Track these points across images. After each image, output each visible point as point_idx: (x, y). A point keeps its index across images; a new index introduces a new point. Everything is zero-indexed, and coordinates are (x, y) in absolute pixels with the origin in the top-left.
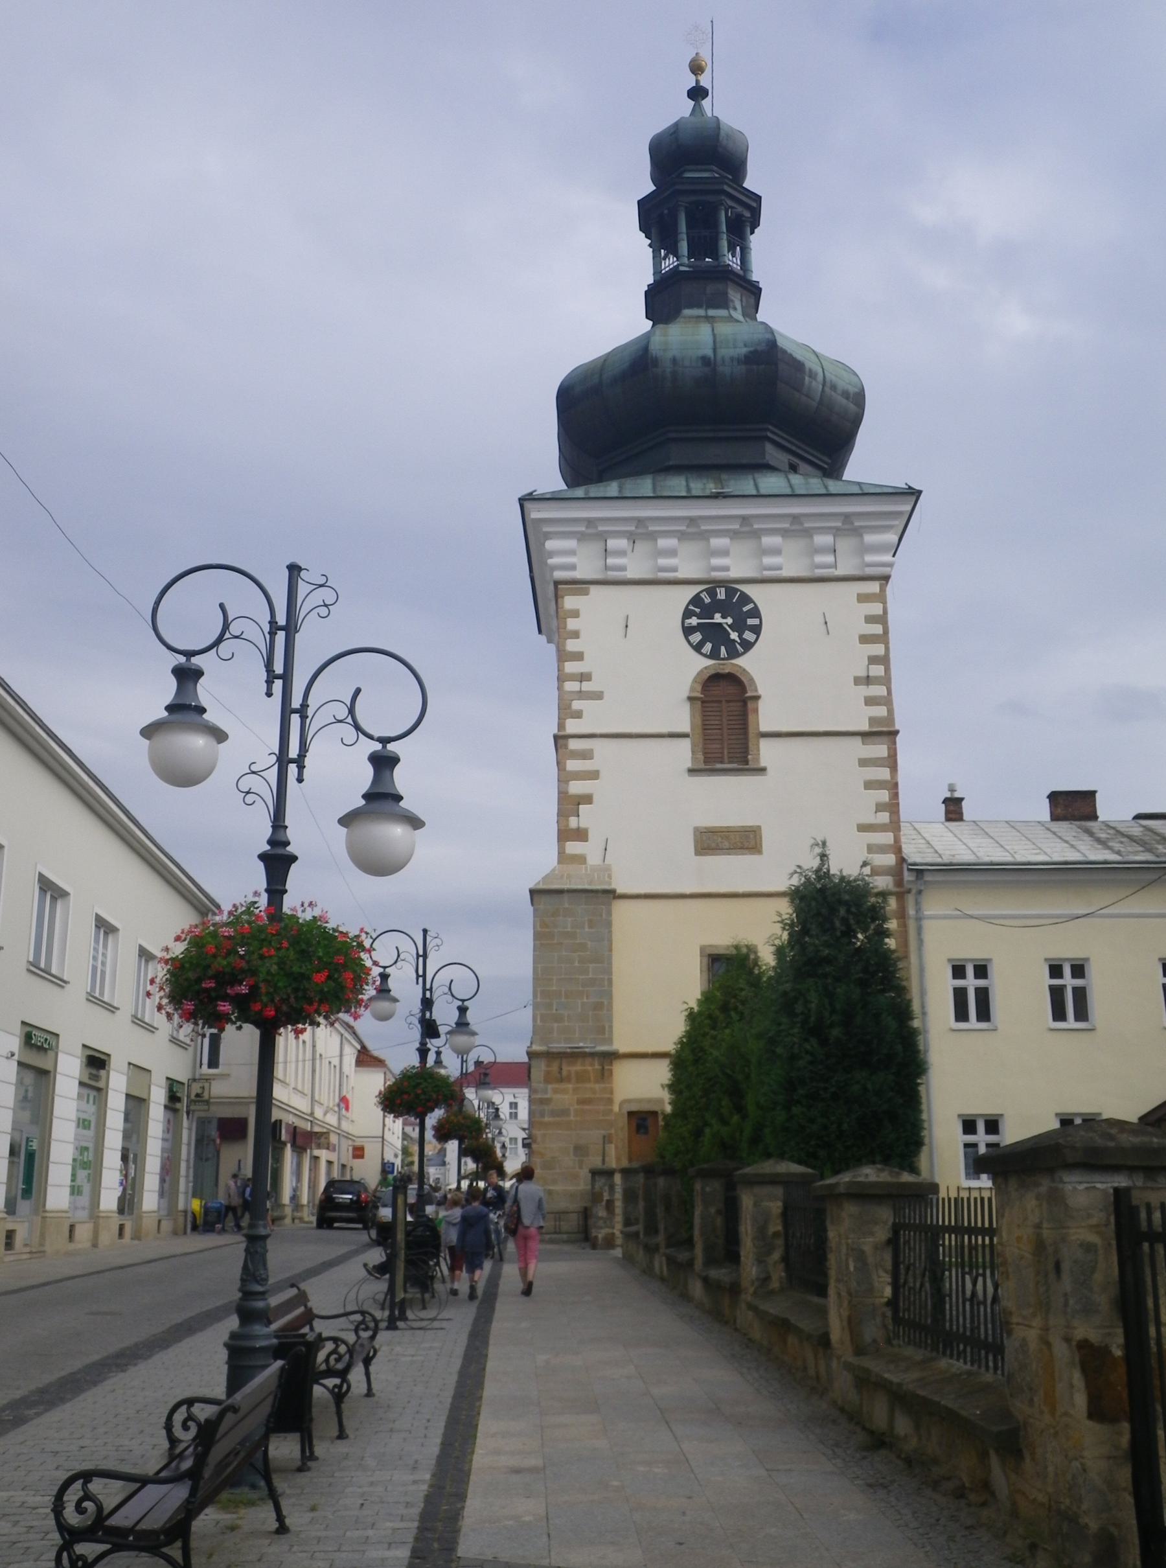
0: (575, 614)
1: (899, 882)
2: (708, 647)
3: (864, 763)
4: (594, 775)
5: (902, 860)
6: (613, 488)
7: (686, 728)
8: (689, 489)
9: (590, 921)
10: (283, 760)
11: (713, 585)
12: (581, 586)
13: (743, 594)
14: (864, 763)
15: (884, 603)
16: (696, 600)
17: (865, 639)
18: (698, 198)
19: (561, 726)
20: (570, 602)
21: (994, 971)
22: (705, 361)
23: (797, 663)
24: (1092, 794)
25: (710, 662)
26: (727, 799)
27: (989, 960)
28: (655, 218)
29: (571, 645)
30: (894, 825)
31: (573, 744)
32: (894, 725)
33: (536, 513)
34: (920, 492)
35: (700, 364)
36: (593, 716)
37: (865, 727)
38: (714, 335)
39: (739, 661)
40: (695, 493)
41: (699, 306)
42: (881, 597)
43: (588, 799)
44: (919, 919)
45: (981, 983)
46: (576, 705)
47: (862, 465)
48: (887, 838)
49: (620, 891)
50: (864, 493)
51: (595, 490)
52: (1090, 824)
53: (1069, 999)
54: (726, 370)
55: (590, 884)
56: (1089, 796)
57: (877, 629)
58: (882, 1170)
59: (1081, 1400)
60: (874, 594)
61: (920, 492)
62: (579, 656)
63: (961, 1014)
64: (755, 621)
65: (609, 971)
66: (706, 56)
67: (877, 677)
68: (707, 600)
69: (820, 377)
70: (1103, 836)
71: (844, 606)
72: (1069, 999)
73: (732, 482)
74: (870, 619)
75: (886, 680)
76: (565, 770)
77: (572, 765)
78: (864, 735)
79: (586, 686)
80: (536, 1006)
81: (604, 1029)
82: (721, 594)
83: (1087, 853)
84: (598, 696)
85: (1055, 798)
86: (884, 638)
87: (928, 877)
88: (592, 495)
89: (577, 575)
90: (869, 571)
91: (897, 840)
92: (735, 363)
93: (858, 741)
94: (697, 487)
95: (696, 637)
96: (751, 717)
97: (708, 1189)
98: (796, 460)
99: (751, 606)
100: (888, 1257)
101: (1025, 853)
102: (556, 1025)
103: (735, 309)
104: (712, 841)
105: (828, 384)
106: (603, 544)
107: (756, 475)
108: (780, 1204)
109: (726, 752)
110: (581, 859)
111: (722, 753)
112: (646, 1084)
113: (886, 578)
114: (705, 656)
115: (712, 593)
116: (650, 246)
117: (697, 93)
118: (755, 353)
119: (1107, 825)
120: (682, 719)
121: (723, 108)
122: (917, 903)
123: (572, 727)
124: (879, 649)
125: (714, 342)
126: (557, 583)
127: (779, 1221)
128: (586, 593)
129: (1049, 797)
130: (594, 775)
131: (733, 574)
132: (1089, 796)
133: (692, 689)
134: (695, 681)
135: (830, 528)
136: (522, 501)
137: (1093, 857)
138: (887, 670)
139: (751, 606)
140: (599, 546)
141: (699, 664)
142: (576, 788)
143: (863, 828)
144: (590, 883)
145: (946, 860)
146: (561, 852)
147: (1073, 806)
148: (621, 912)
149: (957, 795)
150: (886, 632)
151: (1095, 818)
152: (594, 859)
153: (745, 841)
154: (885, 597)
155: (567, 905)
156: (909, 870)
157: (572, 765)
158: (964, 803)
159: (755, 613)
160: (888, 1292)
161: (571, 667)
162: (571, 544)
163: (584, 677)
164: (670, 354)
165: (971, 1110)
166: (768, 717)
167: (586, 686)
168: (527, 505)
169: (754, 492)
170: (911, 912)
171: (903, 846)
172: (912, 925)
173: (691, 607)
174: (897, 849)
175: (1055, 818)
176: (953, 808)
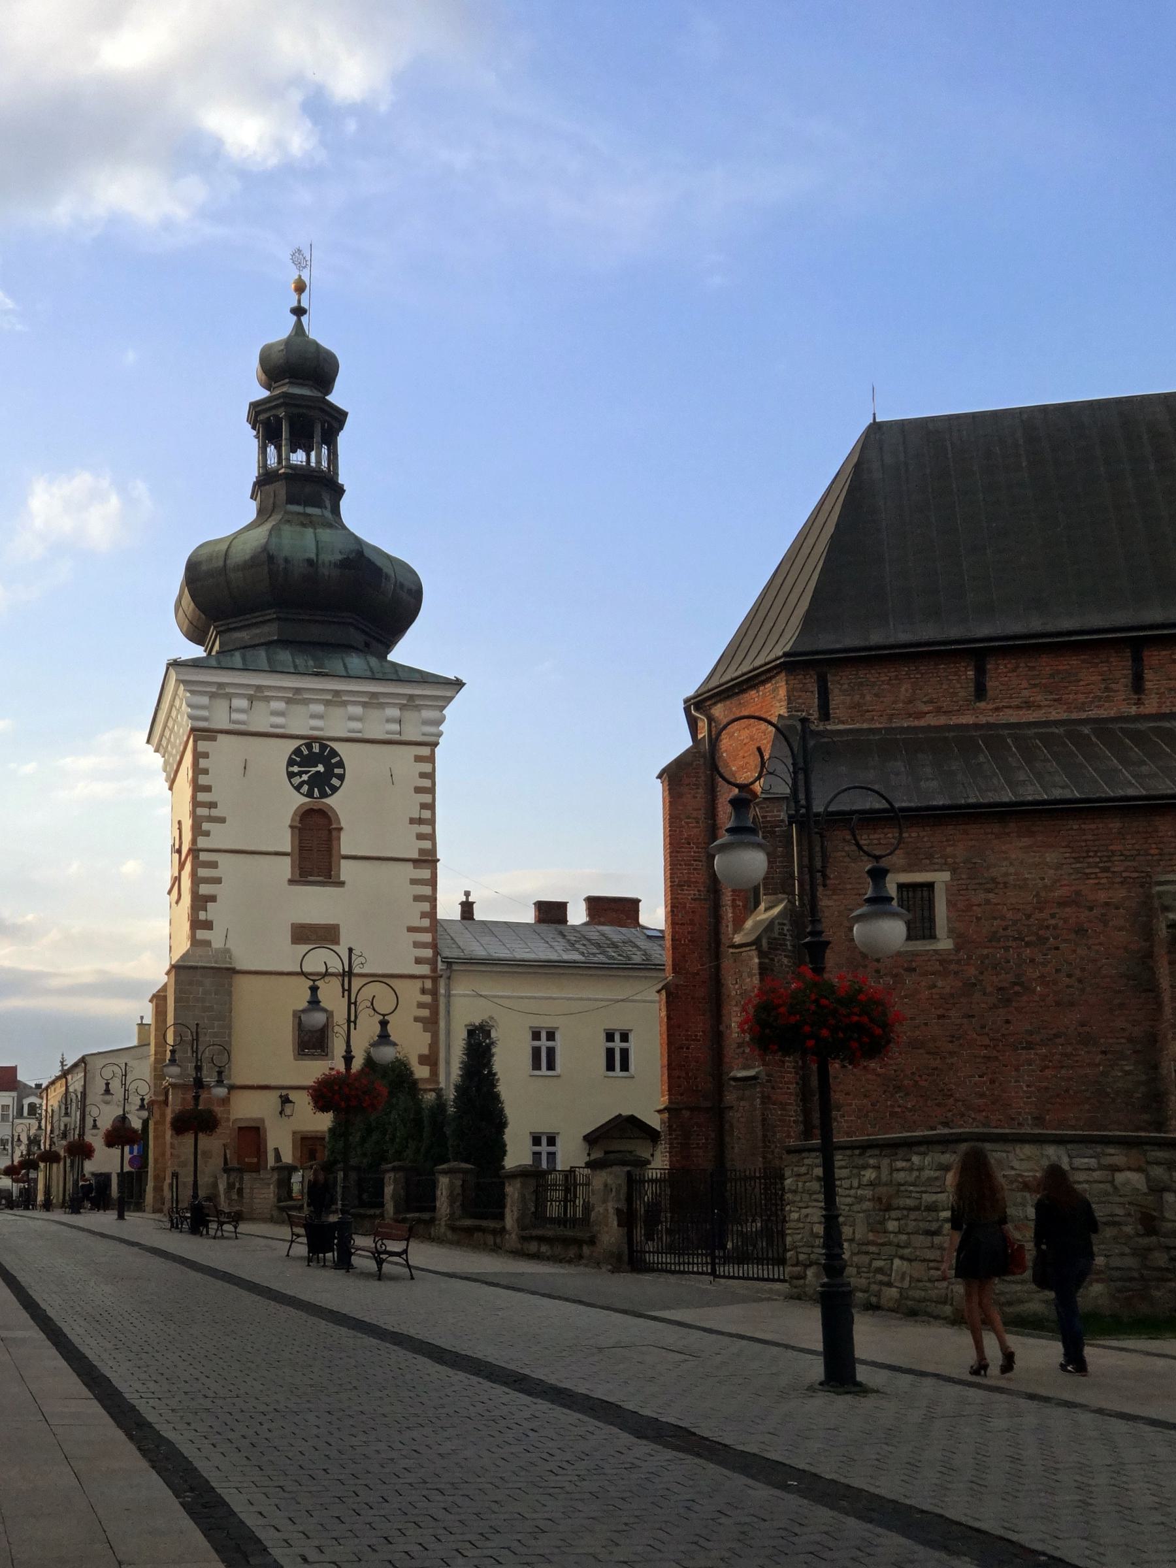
1: (434, 970)
3: (414, 882)
4: (218, 881)
10: (349, 1021)
11: (310, 740)
13: (332, 750)
14: (414, 882)
15: (433, 763)
16: (297, 751)
17: (418, 790)
18: (298, 400)
22: (310, 562)
25: (308, 800)
26: (316, 904)
28: (268, 422)
36: (219, 837)
37: (416, 856)
39: (326, 801)
41: (298, 504)
42: (431, 759)
43: (213, 899)
44: (448, 996)
46: (206, 826)
48: (427, 937)
49: (238, 968)
52: (561, 927)
57: (426, 783)
59: (616, 1223)
65: (230, 1027)
66: (306, 279)
68: (306, 752)
69: (393, 581)
71: (403, 761)
74: (423, 775)
78: (415, 862)
79: (214, 812)
82: (316, 748)
84: (222, 820)
87: (455, 967)
88: (223, 665)
93: (410, 865)
96: (335, 843)
100: (534, 1198)
103: (326, 508)
104: (304, 934)
110: (207, 943)
113: (436, 744)
115: (309, 746)
120: (285, 842)
121: (319, 332)
123: (202, 842)
128: (214, 739)
130: (218, 881)
133: (293, 820)
134: (295, 814)
137: (566, 957)
138: (434, 814)
141: (299, 800)
142: (204, 889)
143: (411, 929)
148: (242, 982)
149: (471, 899)
152: (217, 944)
159: (341, 764)
160: (533, 1209)
163: (212, 805)
165: (539, 1129)
166: (347, 844)
170: (442, 991)
172: (442, 1000)
174: (434, 946)
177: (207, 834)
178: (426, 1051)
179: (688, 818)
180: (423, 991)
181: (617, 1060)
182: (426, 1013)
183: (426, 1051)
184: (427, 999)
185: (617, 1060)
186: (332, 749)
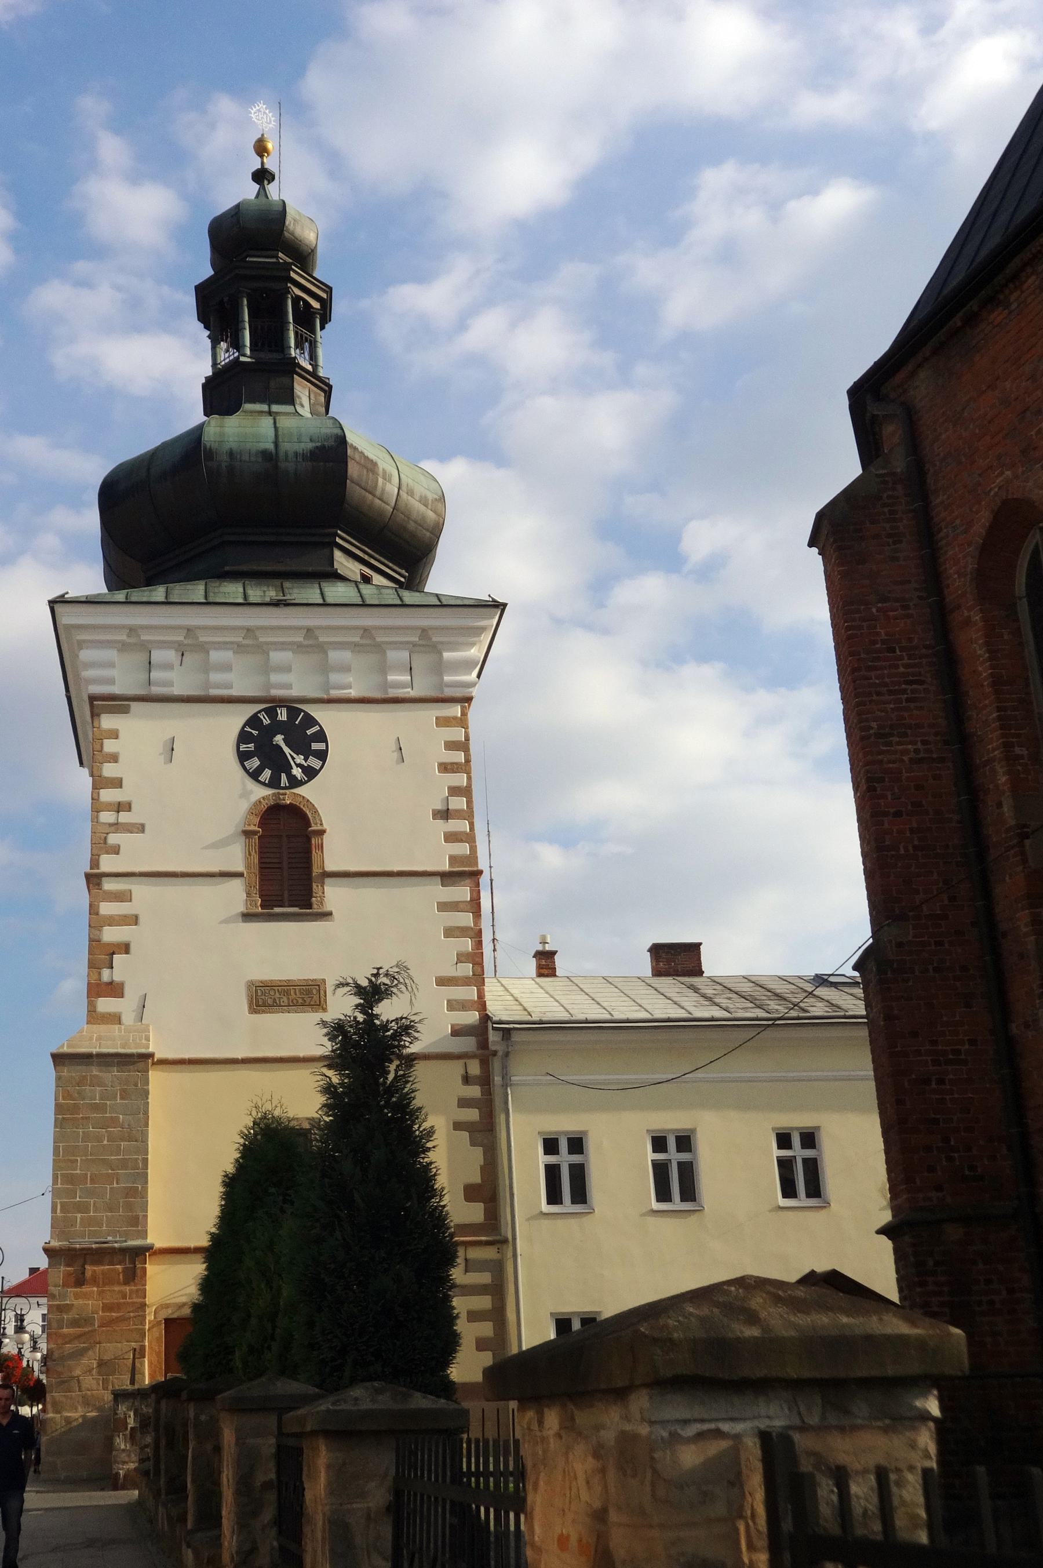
0: (114, 735)
1: (483, 1044)
2: (267, 774)
3: (444, 907)
4: (134, 920)
5: (486, 1018)
6: (159, 593)
7: (240, 867)
8: (245, 596)
9: (123, 1091)
11: (273, 705)
12: (118, 704)
13: (308, 716)
14: (444, 907)
16: (253, 721)
17: (446, 768)
19: (95, 863)
20: (107, 722)
21: (591, 1145)
22: (265, 455)
23: (366, 790)
24: (698, 946)
25: (269, 792)
26: (287, 949)
27: (585, 1133)
28: (215, 308)
29: (109, 770)
30: (478, 979)
31: (109, 885)
32: (476, 864)
33: (69, 616)
34: (505, 605)
35: (260, 460)
36: (132, 853)
37: (446, 867)
38: (276, 428)
40: (252, 600)
41: (262, 402)
42: (462, 722)
45: (576, 1159)
46: (113, 839)
47: (443, 579)
48: (470, 993)
50: (441, 604)
51: (136, 595)
52: (695, 980)
53: (676, 1178)
54: (291, 466)
55: (123, 1047)
56: (693, 949)
57: (460, 757)
58: (378, 1391)
60: (455, 718)
61: (505, 605)
62: (118, 783)
63: (554, 1196)
64: (321, 746)
67: (456, 811)
68: (266, 721)
70: (709, 992)
71: (422, 731)
72: (676, 1178)
73: (296, 591)
74: (451, 746)
75: (468, 815)
76: (97, 914)
77: (107, 908)
80: (56, 1193)
81: (137, 1222)
82: (283, 715)
83: (691, 1009)
84: (141, 828)
85: (658, 951)
86: (465, 767)
87: (516, 1037)
88: (133, 599)
89: (115, 690)
90: (448, 692)
91: (481, 995)
92: (300, 459)
94: (255, 594)
95: (254, 763)
97: (203, 1418)
98: (368, 571)
99: (316, 728)
101: (624, 1010)
102: (79, 1215)
103: (302, 406)
104: (266, 997)
105: (404, 488)
106: (146, 656)
107: (323, 584)
108: (273, 1441)
109: (286, 895)
110: (115, 1019)
111: (282, 895)
112: (173, 1285)
113: (469, 700)
114: (264, 784)
115: (271, 712)
116: (209, 337)
117: (262, 176)
118: (322, 449)
119: (713, 980)
120: (236, 857)
122: (504, 1067)
124: (461, 780)
125: (276, 436)
126: (92, 698)
127: (272, 1465)
128: (125, 710)
129: (650, 950)
131: (295, 692)
132: (693, 949)
134: (251, 812)
135: (407, 643)
136: (52, 603)
137: (698, 1013)
138: (470, 803)
139: (316, 728)
140: (140, 658)
142: (111, 935)
144: (123, 1047)
145: (535, 1018)
146: (92, 1010)
147: (677, 960)
148: (156, 1078)
149: (548, 948)
150: (468, 761)
151: (700, 973)
153: (306, 996)
154: (466, 720)
155: (95, 1073)
156: (494, 1029)
157: (107, 908)
158: (556, 957)
159: (321, 736)
161: (107, 795)
162: (111, 654)
163: (121, 807)
164: (226, 447)
166: (335, 853)
167: (124, 817)
168: (58, 608)
169: (321, 601)
170: (497, 1079)
171: (488, 1003)
173: (248, 729)
175: (657, 973)
176: (546, 963)
177: (116, 850)
178: (476, 1178)
179: (885, 600)
180: (467, 1080)
181: (801, 1175)
182: (472, 1115)
183: (476, 1178)
184: (474, 1091)
185: (801, 1175)
186: (307, 715)
